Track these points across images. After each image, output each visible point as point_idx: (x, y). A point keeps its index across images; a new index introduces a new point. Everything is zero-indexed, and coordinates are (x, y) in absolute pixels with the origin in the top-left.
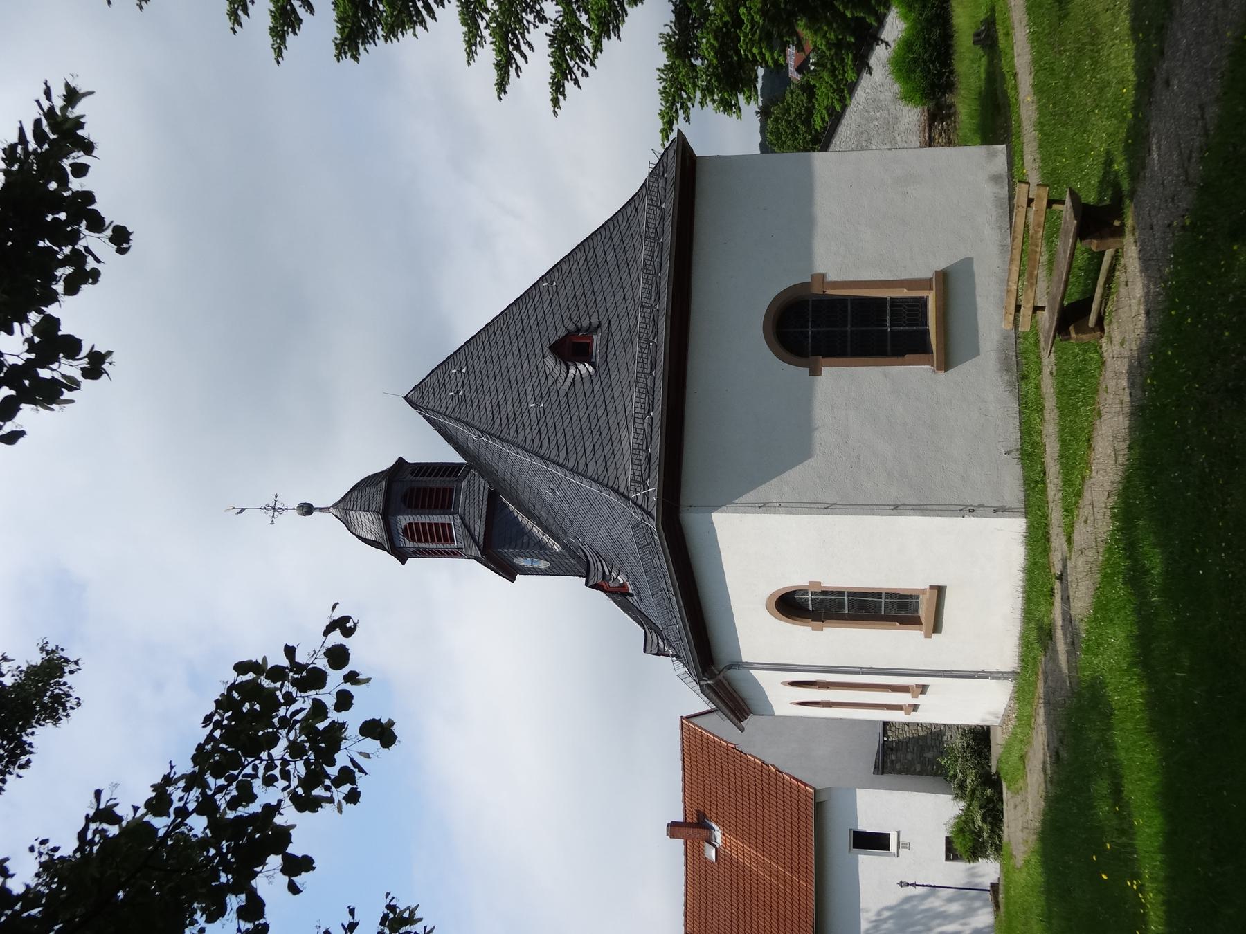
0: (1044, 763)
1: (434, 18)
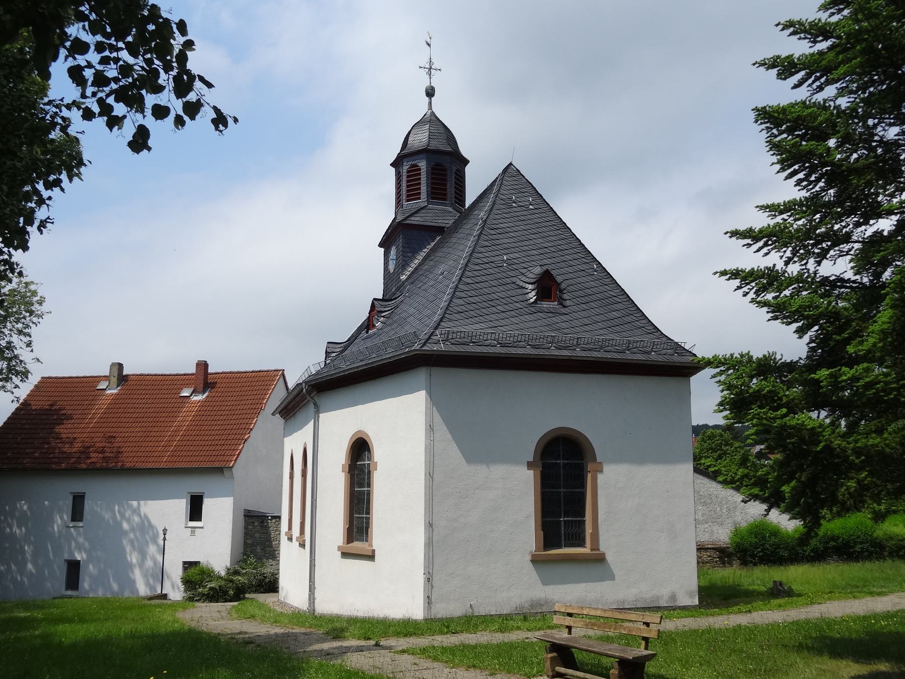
0: (246, 633)
1: (787, 178)
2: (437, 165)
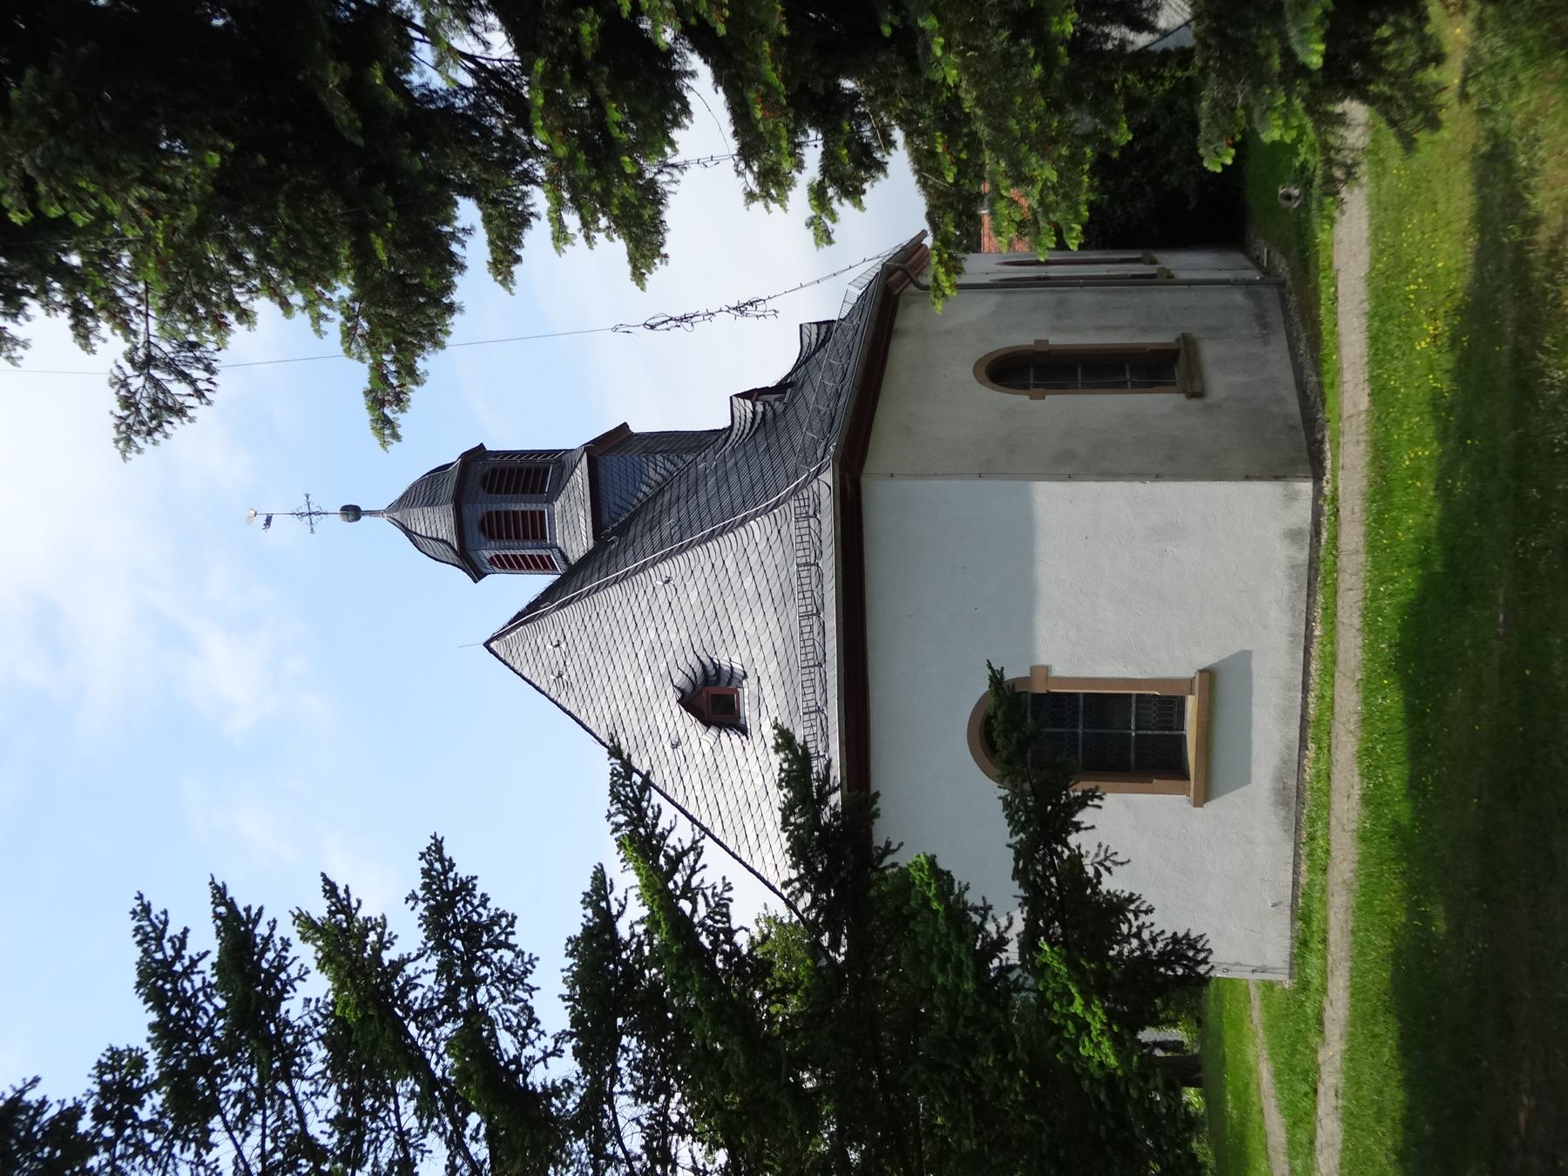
2: (482, 528)
